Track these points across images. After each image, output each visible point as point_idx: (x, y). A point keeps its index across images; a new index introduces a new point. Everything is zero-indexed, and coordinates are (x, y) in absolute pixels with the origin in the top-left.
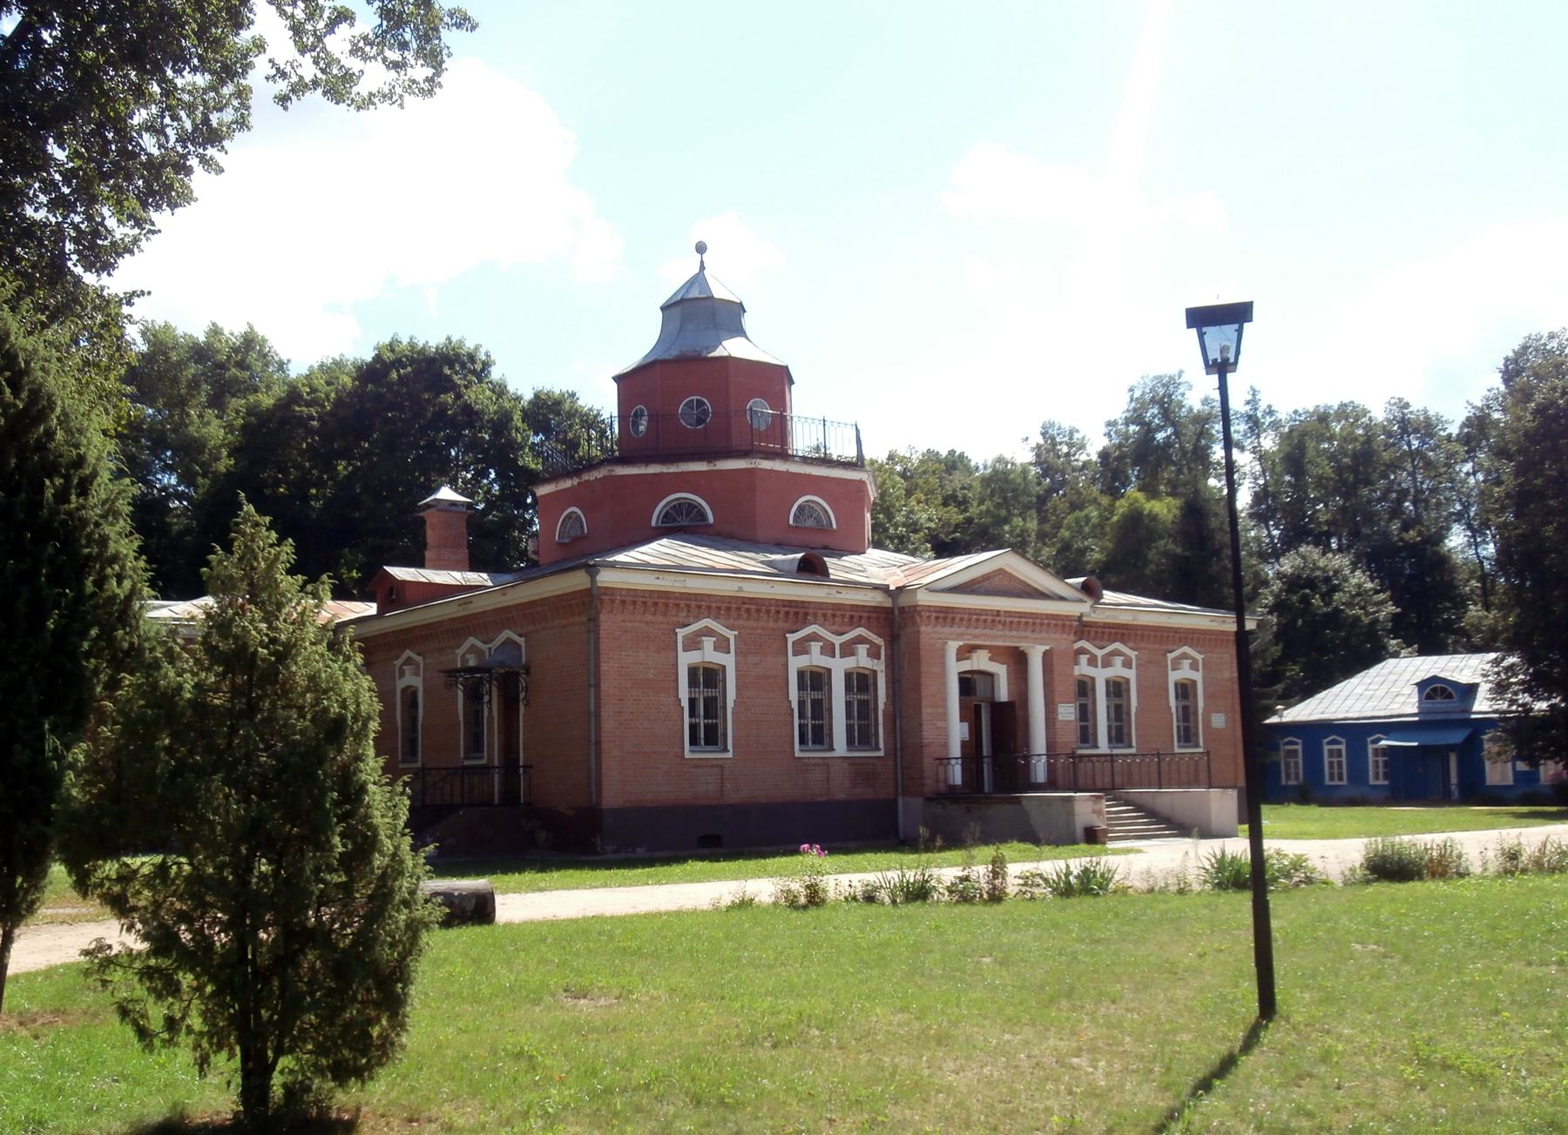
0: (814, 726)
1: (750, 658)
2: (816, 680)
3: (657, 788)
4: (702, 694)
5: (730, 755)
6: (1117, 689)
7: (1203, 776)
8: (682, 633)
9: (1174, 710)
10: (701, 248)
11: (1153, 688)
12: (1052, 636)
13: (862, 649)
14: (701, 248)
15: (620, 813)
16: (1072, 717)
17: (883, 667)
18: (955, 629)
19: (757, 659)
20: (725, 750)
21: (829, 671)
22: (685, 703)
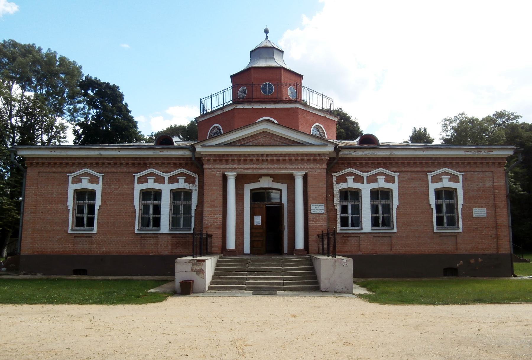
0: (88, 218)
1: (113, 186)
2: (151, 196)
3: (54, 246)
4: (444, 203)
5: (395, 230)
6: (380, 196)
7: (326, 252)
8: (430, 175)
9: (71, 208)
10: (266, 31)
11: (414, 196)
12: (307, 166)
13: (182, 180)
14: (266, 31)
15: (28, 257)
16: (323, 212)
17: (197, 188)
18: (231, 166)
19: (117, 187)
20: (458, 228)
21: (456, 189)
22: (434, 207)
